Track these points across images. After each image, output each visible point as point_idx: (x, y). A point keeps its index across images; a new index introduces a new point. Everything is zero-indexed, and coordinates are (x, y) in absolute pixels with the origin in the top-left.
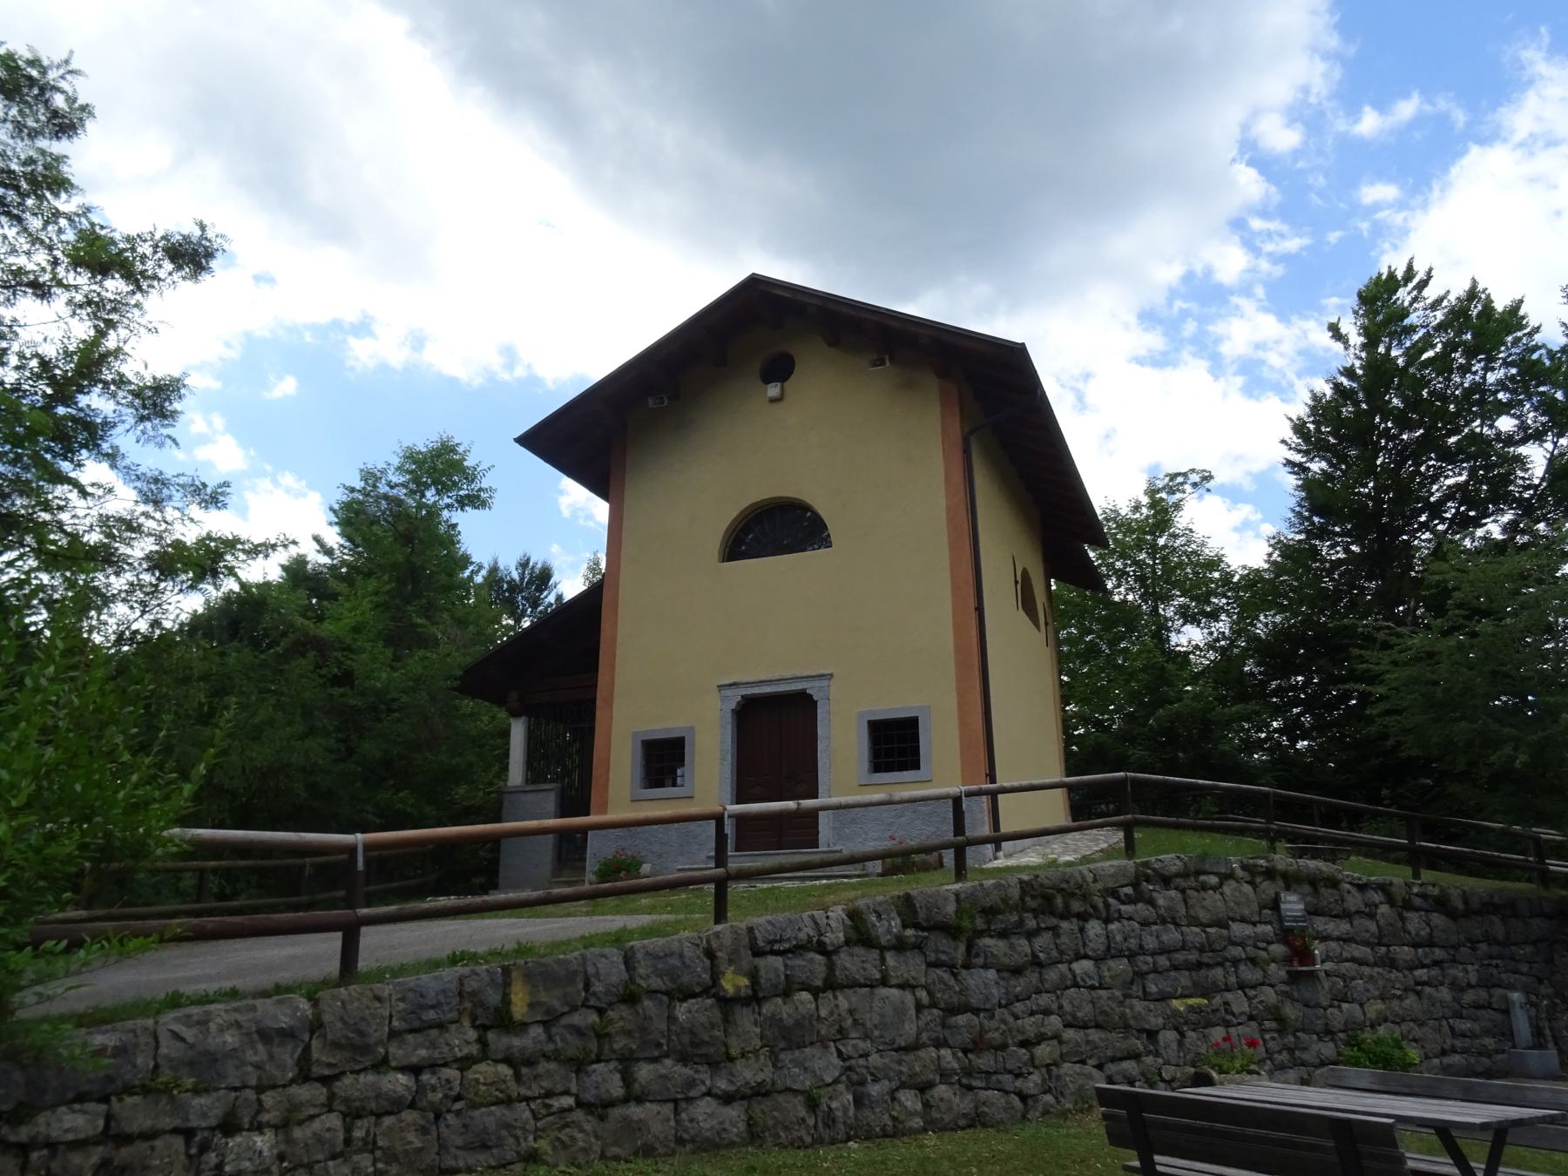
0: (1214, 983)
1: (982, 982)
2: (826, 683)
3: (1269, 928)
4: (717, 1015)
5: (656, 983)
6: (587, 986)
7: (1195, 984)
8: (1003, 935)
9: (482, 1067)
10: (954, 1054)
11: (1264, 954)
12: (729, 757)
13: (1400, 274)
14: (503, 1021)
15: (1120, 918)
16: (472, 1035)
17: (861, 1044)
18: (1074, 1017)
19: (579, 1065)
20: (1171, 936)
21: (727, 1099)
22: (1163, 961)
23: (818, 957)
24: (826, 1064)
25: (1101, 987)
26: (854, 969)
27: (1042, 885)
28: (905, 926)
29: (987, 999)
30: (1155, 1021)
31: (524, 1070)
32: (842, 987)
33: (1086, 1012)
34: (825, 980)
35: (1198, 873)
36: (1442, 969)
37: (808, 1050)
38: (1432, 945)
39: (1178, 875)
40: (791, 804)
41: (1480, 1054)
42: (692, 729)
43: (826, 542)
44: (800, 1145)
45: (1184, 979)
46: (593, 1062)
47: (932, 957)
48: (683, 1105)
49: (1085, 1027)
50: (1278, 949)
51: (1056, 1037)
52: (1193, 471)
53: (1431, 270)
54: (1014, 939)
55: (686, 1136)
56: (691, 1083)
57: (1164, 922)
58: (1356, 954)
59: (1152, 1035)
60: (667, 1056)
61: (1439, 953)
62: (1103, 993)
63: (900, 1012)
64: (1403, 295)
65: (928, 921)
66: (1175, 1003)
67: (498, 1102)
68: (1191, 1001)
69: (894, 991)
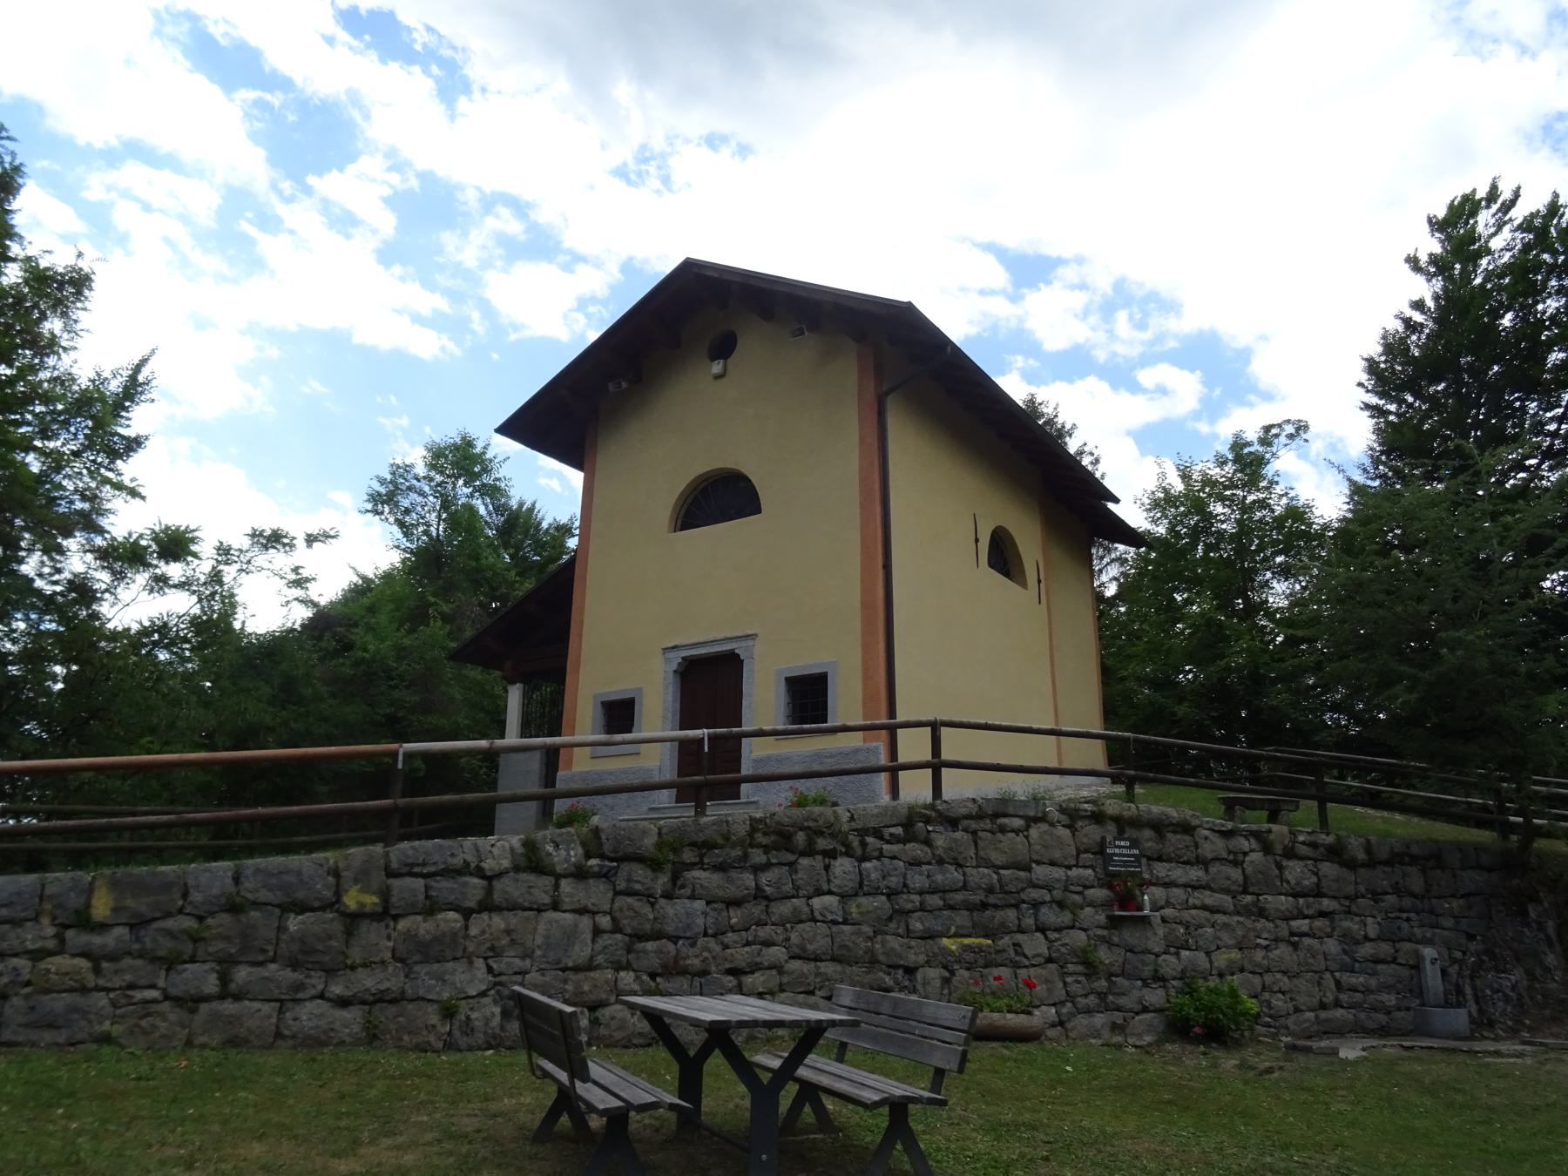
0: (1003, 924)
1: (683, 911)
2: (751, 643)
3: (1090, 871)
4: (338, 927)
5: (265, 895)
6: (185, 896)
7: (974, 925)
8: (721, 868)
9: (58, 959)
10: (637, 978)
11: (1077, 898)
12: (670, 715)
13: (1481, 193)
14: (84, 921)
15: (880, 856)
16: (51, 931)
17: (518, 962)
18: (804, 949)
19: (170, 963)
20: (953, 875)
21: (343, 1003)
22: (934, 901)
23: (476, 881)
24: (472, 978)
25: (845, 922)
26: (517, 893)
27: (779, 823)
28: (588, 856)
29: (688, 926)
30: (912, 958)
31: (105, 965)
32: (499, 909)
33: (820, 944)
34: (480, 903)
35: (996, 815)
36: (1332, 921)
37: (449, 965)
38: (1319, 894)
39: (968, 817)
40: (484, 743)
41: (1375, 1009)
42: (640, 690)
43: (756, 509)
44: (423, 1048)
45: (962, 918)
46: (186, 962)
47: (622, 885)
48: (289, 1005)
49: (817, 959)
50: (1099, 894)
51: (778, 968)
52: (1288, 421)
53: (1519, 188)
54: (734, 874)
55: (286, 1032)
56: (300, 987)
57: (941, 862)
58: (1208, 901)
59: (910, 971)
60: (273, 961)
61: (1327, 904)
62: (846, 928)
63: (571, 935)
64: (1484, 220)
65: (614, 851)
66: (945, 941)
67: (71, 990)
68: (967, 941)
69: (568, 916)
